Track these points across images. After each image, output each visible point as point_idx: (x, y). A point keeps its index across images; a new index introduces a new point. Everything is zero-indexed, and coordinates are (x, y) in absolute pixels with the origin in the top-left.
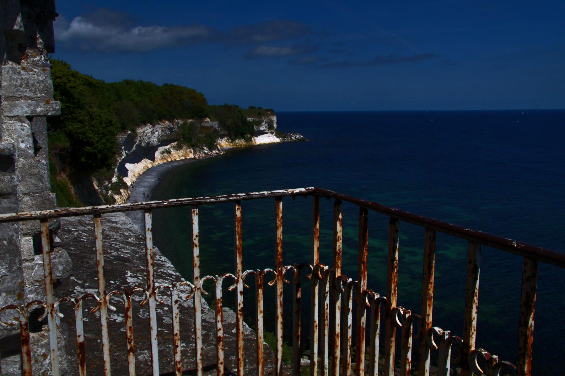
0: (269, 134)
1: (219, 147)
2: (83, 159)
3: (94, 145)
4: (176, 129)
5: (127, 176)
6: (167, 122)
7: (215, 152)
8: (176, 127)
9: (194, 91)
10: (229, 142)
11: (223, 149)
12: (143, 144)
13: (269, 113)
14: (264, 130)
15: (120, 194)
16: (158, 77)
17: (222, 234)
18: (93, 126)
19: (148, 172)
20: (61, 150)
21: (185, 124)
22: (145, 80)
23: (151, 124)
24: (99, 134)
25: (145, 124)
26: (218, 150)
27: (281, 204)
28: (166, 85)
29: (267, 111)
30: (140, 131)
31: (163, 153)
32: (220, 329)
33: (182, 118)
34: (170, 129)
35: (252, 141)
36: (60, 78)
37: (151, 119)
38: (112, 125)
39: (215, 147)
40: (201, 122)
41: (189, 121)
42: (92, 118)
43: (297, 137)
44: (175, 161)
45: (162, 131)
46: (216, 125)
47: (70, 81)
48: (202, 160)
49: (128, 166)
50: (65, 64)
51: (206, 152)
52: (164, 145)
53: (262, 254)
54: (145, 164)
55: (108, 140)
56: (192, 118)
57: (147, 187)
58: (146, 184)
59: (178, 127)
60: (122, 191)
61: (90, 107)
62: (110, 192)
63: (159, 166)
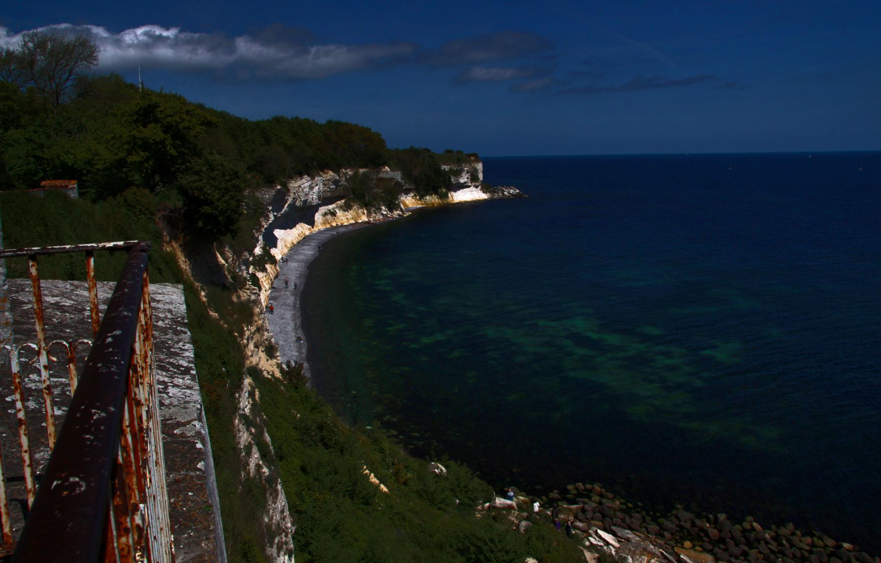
0: (472, 188)
1: (402, 206)
2: (201, 224)
3: (213, 203)
4: (343, 181)
5: (276, 247)
6: (331, 173)
7: (396, 213)
8: (344, 179)
9: (368, 130)
10: (416, 200)
11: (408, 210)
12: (298, 204)
13: (472, 158)
14: (465, 183)
15: (264, 270)
16: (320, 113)
17: (402, 326)
18: (214, 179)
19: (305, 240)
20: (171, 211)
21: (356, 174)
22: (302, 117)
23: (309, 175)
24: (220, 189)
25: (301, 176)
26: (402, 210)
27: (92, 260)
28: (330, 122)
29: (470, 155)
30: (293, 185)
31: (325, 214)
32: (20, 410)
33: (351, 167)
34: (336, 182)
35: (448, 197)
36: (171, 116)
37: (309, 169)
38: (238, 177)
39: (397, 207)
40: (379, 172)
41: (361, 171)
42: (212, 168)
43: (512, 191)
44: (342, 226)
45: (325, 185)
46: (398, 176)
47: (183, 120)
48: (379, 224)
49: (278, 233)
50: (180, 98)
51: (385, 213)
52: (327, 205)
53: (456, 354)
54: (302, 230)
55: (232, 198)
56: (366, 167)
57: (302, 261)
58: (301, 257)
59: (347, 180)
60: (268, 266)
61: (211, 153)
62: (251, 267)
63: (320, 232)
